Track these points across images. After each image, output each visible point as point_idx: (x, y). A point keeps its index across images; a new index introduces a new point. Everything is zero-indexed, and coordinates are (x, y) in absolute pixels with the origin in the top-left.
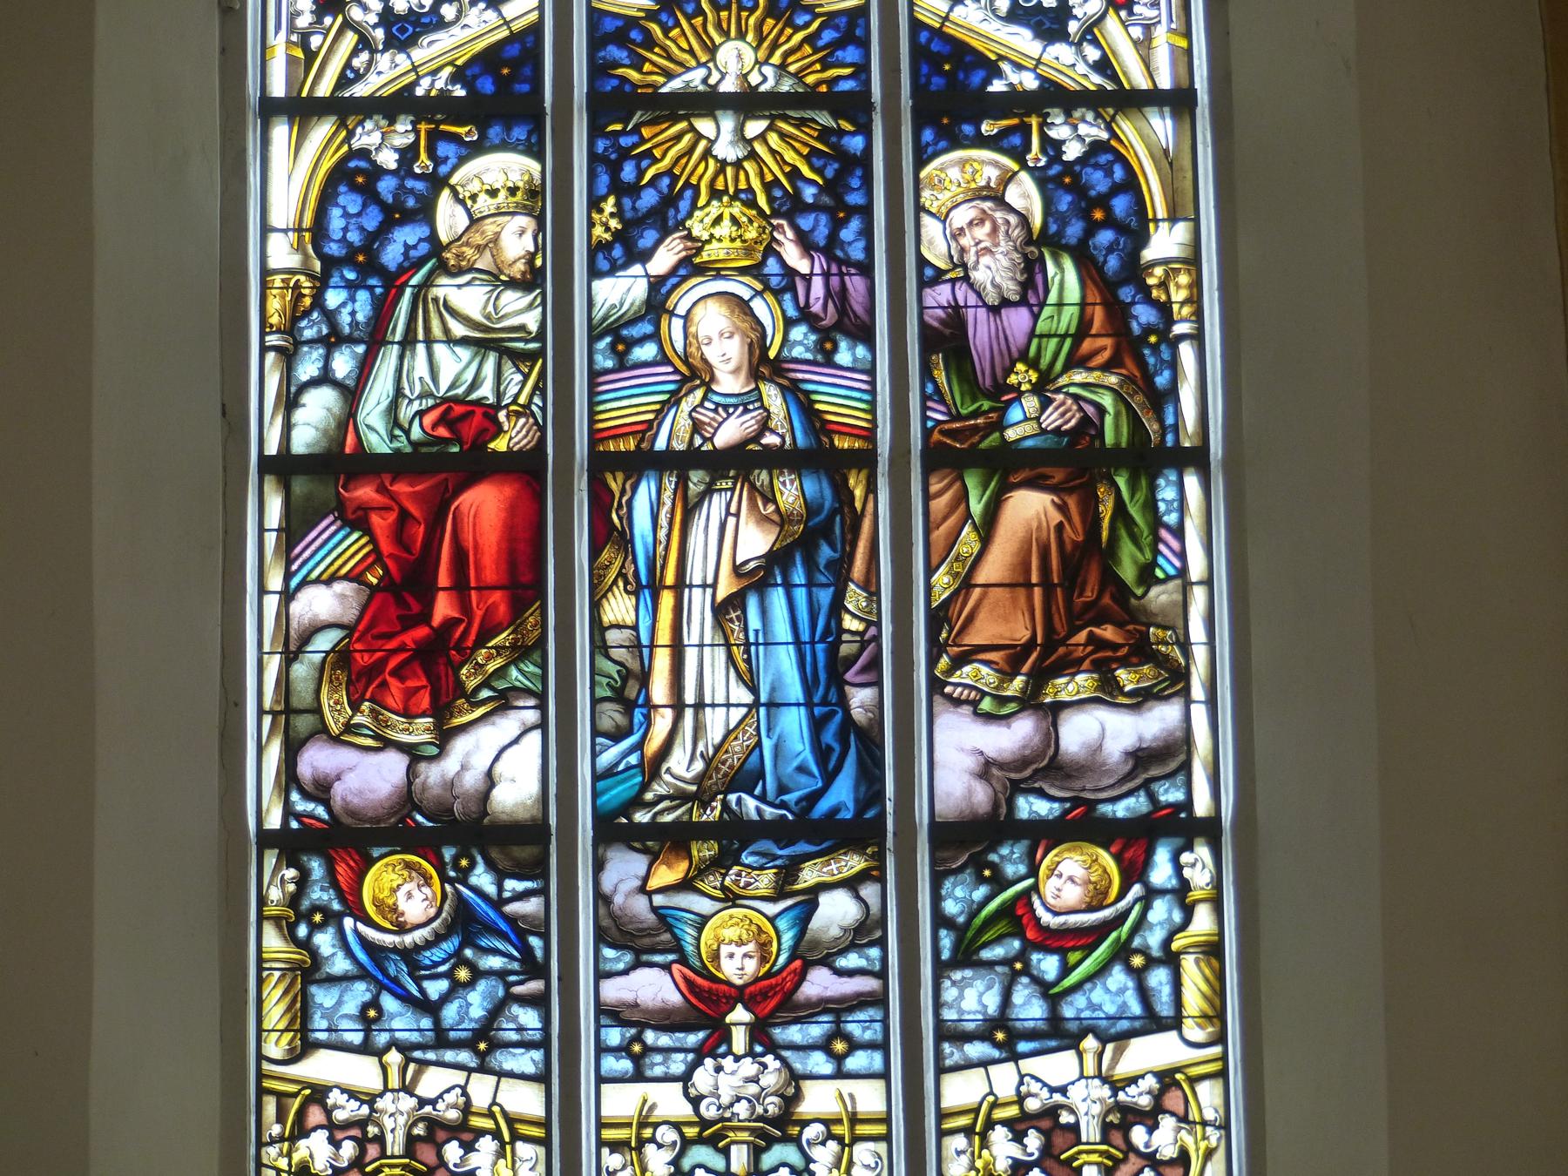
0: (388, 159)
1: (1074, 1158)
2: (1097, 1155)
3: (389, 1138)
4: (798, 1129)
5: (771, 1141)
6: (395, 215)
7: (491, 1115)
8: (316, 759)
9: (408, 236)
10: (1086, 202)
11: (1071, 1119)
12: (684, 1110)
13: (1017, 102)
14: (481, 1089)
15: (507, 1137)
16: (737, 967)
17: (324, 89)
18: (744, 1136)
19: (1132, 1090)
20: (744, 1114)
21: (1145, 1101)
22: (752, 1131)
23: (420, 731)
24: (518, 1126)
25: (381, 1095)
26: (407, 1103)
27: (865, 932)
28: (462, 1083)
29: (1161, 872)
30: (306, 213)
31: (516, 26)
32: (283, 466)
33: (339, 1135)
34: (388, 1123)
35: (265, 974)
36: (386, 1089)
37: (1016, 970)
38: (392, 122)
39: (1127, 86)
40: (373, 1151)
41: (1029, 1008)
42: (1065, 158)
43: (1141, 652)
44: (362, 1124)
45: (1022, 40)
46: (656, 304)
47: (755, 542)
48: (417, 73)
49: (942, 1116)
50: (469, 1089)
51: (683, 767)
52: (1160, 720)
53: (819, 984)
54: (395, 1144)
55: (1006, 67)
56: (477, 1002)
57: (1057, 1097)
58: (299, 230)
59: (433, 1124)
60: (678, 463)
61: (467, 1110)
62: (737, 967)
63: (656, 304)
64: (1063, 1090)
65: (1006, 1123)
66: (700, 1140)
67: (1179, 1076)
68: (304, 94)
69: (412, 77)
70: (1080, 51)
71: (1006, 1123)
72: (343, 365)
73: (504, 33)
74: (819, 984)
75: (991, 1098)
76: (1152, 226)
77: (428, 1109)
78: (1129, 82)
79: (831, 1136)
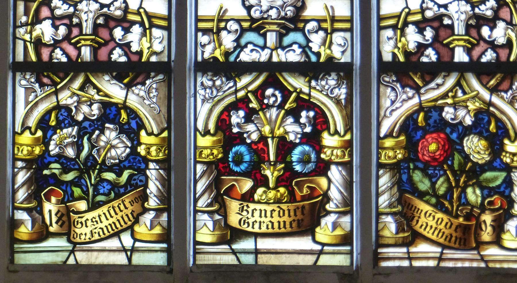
1: (450, 43)
3: (84, 25)
4: (303, 24)
5: (289, 31)
7: (139, 13)
11: (449, 22)
22: (279, 25)
24: (153, 20)
33: (58, 23)
34: (84, 17)
40: (75, 31)
49: (380, 19)
54: (88, 28)
57: (442, 10)
59: (108, 18)
65: (415, 23)
66: (250, 29)
75: (407, 10)
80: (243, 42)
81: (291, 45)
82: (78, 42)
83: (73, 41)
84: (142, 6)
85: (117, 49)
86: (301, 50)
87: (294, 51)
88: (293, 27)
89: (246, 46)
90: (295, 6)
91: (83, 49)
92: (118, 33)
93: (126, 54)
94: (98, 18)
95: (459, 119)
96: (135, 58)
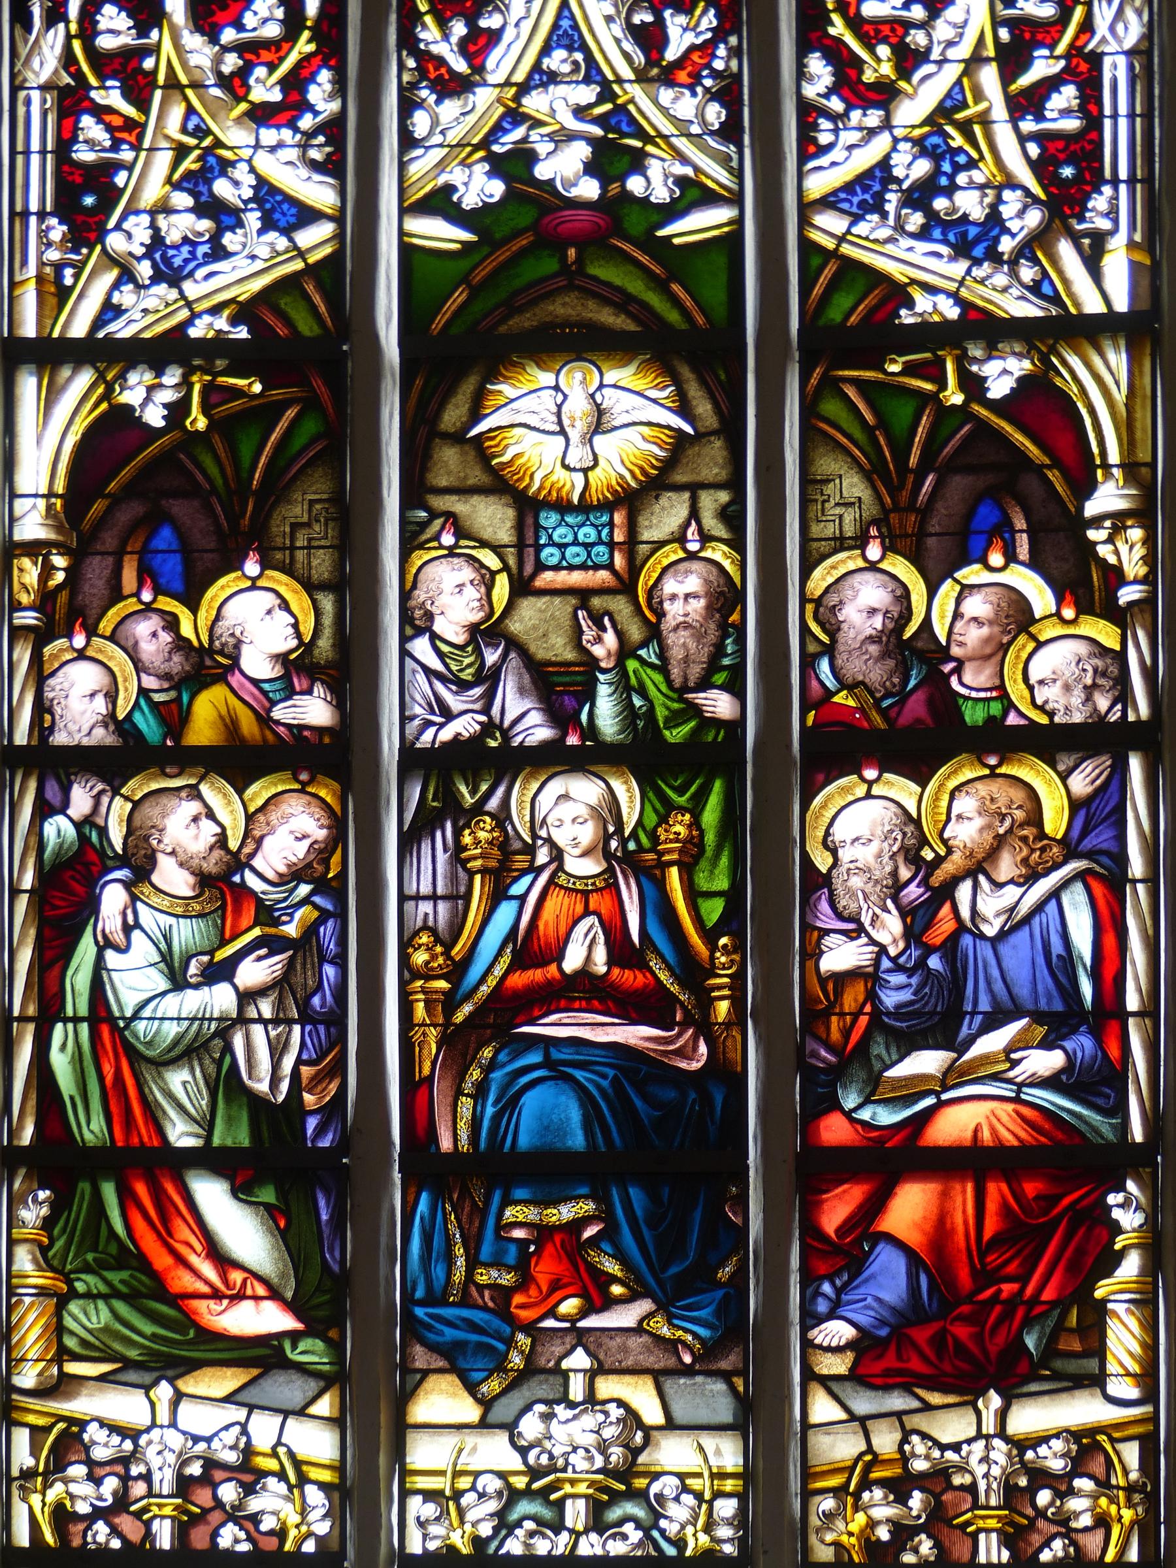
0: (155, 417)
1: (968, 1523)
2: (995, 1521)
3: (156, 1477)
4: (647, 1481)
5: (615, 1497)
7: (274, 1454)
11: (967, 1479)
12: (514, 1462)
14: (263, 1430)
15: (293, 1479)
17: (79, 329)
18: (582, 1488)
19: (1043, 1450)
20: (582, 1465)
21: (1057, 1465)
22: (592, 1484)
24: (305, 1468)
25: (148, 1430)
26: (175, 1440)
28: (243, 1421)
30: (57, 481)
31: (313, 258)
33: (100, 1472)
34: (155, 1462)
35: (14, 1300)
36: (154, 1425)
38: (159, 373)
39: (1073, 311)
40: (139, 1489)
42: (990, 395)
44: (125, 1461)
48: (191, 310)
49: (807, 1474)
50: (251, 1428)
54: (165, 1481)
55: (917, 295)
57: (950, 1455)
58: (50, 495)
59: (210, 1464)
61: (248, 1452)
64: (956, 1447)
65: (882, 1483)
66: (528, 1493)
67: (1102, 1438)
68: (55, 334)
69: (184, 314)
70: (1014, 274)
71: (882, 1483)
73: (298, 265)
75: (868, 1458)
76: (1099, 472)
77: (202, 1446)
78: (1077, 305)
79: (685, 1489)
80: (514, 1516)
81: (621, 1522)
82: (145, 1510)
83: (133, 1508)
84: (283, 1440)
85: (230, 1525)
86: (640, 1534)
87: (625, 1537)
88: (623, 1487)
89: (519, 1524)
90: (626, 1446)
91: (156, 1525)
92: (228, 1492)
93: (250, 1538)
94: (185, 1463)
95: (437, 1261)
96: (271, 1544)
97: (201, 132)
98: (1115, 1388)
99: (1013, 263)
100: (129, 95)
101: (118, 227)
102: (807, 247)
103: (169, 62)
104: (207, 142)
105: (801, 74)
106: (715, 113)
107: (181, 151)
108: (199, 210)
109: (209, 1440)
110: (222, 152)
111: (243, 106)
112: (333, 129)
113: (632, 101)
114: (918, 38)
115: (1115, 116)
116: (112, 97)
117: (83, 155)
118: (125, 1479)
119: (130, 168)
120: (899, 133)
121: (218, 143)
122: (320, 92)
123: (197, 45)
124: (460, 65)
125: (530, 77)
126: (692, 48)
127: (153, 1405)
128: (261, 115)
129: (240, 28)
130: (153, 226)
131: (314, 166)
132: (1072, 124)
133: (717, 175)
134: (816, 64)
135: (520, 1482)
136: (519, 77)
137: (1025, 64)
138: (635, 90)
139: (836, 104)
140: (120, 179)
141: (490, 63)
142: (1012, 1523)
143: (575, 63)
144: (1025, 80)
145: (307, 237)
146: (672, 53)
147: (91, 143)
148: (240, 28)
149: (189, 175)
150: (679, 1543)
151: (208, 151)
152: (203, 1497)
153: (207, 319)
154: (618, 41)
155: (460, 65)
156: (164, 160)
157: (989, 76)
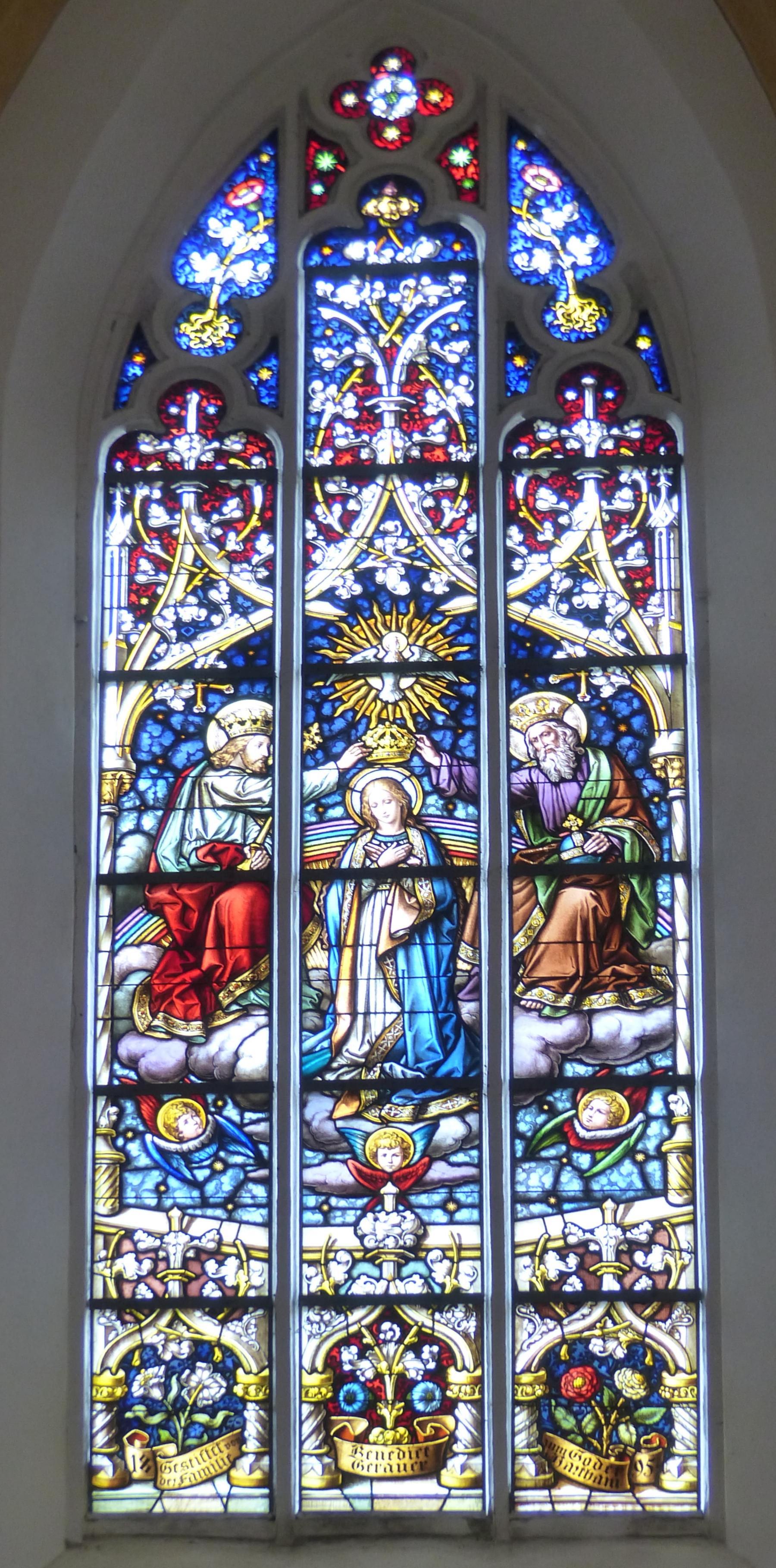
1: (598, 1270)
3: (172, 1258)
5: (408, 1260)
6: (182, 736)
7: (234, 1245)
8: (129, 1046)
9: (187, 748)
10: (614, 721)
11: (597, 1248)
12: (355, 1243)
13: (572, 664)
16: (389, 1162)
17: (139, 666)
21: (644, 1238)
22: (397, 1254)
23: (194, 1029)
27: (469, 1141)
29: (656, 1106)
32: (111, 881)
33: (141, 1257)
34: (171, 1250)
37: (562, 1163)
41: (571, 1184)
43: (645, 980)
45: (576, 628)
46: (343, 785)
47: (403, 919)
49: (515, 1246)
50: (222, 1231)
51: (356, 1047)
52: (657, 1019)
53: (439, 1171)
56: (227, 1182)
58: (123, 746)
60: (355, 875)
61: (220, 1242)
62: (389, 1162)
63: (343, 785)
65: (554, 1250)
66: (364, 1260)
67: (665, 1223)
69: (193, 658)
71: (554, 1250)
72: (149, 822)
74: (439, 1171)
75: (546, 1236)
77: (196, 1242)
79: (445, 1257)
80: (355, 1273)
82: (165, 1276)
89: (358, 1277)
93: (220, 1289)
96: (230, 1293)
97: (204, 565)
98: (673, 1197)
99: (612, 630)
100: (165, 548)
101: (159, 614)
102: (509, 621)
103: (186, 536)
104: (206, 570)
105: (506, 536)
106: (468, 551)
107: (192, 576)
108: (200, 605)
109: (200, 1238)
110: (212, 576)
111: (223, 552)
112: (269, 563)
113: (425, 545)
114: (563, 520)
115: (661, 558)
116: (156, 549)
117: (141, 578)
118: (156, 1261)
119: (165, 584)
120: (556, 566)
121: (211, 571)
122: (263, 544)
123: (200, 525)
124: (338, 528)
125: (374, 533)
126: (454, 520)
127: (169, 1219)
128: (233, 558)
129: (221, 514)
130: (176, 613)
131: (260, 582)
132: (641, 562)
133: (468, 581)
134: (514, 530)
135: (358, 1255)
136: (369, 534)
137: (618, 531)
138: (427, 540)
139: (523, 550)
140: (160, 590)
141: (354, 527)
142: (621, 1269)
143: (396, 526)
144: (616, 541)
145: (255, 617)
146: (446, 523)
147: (145, 572)
148: (221, 514)
149: (196, 588)
150: (443, 1286)
151: (206, 575)
152: (195, 1267)
153: (203, 659)
154: (418, 516)
155: (338, 528)
156: (183, 579)
157: (599, 538)
